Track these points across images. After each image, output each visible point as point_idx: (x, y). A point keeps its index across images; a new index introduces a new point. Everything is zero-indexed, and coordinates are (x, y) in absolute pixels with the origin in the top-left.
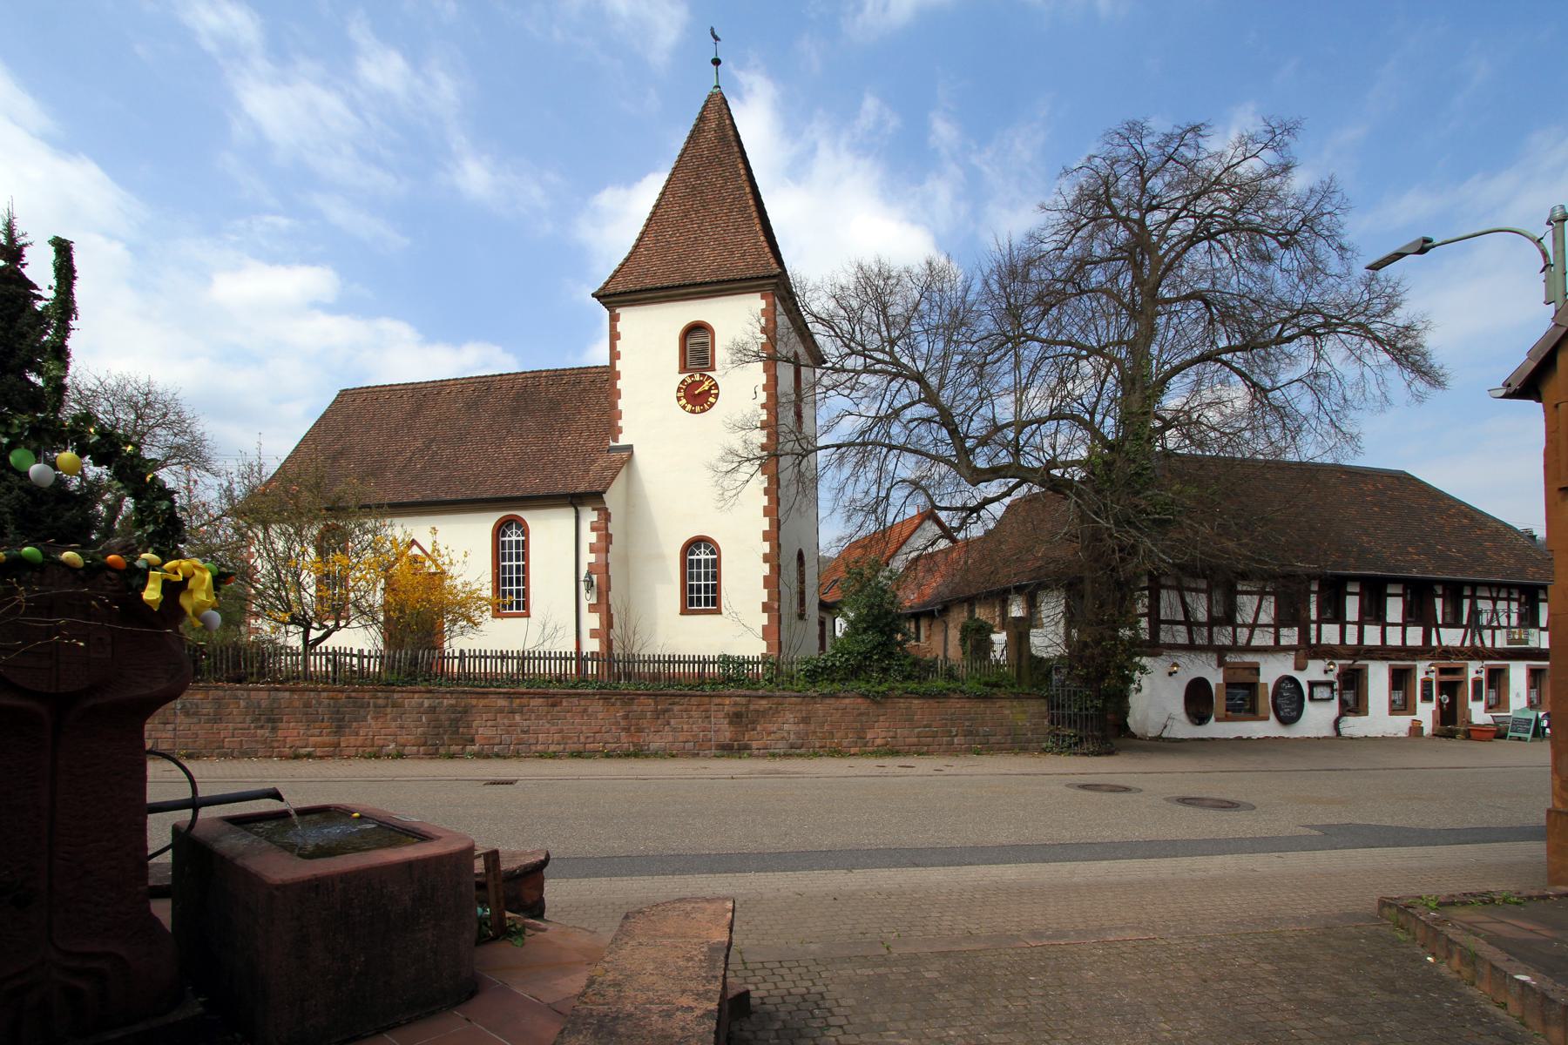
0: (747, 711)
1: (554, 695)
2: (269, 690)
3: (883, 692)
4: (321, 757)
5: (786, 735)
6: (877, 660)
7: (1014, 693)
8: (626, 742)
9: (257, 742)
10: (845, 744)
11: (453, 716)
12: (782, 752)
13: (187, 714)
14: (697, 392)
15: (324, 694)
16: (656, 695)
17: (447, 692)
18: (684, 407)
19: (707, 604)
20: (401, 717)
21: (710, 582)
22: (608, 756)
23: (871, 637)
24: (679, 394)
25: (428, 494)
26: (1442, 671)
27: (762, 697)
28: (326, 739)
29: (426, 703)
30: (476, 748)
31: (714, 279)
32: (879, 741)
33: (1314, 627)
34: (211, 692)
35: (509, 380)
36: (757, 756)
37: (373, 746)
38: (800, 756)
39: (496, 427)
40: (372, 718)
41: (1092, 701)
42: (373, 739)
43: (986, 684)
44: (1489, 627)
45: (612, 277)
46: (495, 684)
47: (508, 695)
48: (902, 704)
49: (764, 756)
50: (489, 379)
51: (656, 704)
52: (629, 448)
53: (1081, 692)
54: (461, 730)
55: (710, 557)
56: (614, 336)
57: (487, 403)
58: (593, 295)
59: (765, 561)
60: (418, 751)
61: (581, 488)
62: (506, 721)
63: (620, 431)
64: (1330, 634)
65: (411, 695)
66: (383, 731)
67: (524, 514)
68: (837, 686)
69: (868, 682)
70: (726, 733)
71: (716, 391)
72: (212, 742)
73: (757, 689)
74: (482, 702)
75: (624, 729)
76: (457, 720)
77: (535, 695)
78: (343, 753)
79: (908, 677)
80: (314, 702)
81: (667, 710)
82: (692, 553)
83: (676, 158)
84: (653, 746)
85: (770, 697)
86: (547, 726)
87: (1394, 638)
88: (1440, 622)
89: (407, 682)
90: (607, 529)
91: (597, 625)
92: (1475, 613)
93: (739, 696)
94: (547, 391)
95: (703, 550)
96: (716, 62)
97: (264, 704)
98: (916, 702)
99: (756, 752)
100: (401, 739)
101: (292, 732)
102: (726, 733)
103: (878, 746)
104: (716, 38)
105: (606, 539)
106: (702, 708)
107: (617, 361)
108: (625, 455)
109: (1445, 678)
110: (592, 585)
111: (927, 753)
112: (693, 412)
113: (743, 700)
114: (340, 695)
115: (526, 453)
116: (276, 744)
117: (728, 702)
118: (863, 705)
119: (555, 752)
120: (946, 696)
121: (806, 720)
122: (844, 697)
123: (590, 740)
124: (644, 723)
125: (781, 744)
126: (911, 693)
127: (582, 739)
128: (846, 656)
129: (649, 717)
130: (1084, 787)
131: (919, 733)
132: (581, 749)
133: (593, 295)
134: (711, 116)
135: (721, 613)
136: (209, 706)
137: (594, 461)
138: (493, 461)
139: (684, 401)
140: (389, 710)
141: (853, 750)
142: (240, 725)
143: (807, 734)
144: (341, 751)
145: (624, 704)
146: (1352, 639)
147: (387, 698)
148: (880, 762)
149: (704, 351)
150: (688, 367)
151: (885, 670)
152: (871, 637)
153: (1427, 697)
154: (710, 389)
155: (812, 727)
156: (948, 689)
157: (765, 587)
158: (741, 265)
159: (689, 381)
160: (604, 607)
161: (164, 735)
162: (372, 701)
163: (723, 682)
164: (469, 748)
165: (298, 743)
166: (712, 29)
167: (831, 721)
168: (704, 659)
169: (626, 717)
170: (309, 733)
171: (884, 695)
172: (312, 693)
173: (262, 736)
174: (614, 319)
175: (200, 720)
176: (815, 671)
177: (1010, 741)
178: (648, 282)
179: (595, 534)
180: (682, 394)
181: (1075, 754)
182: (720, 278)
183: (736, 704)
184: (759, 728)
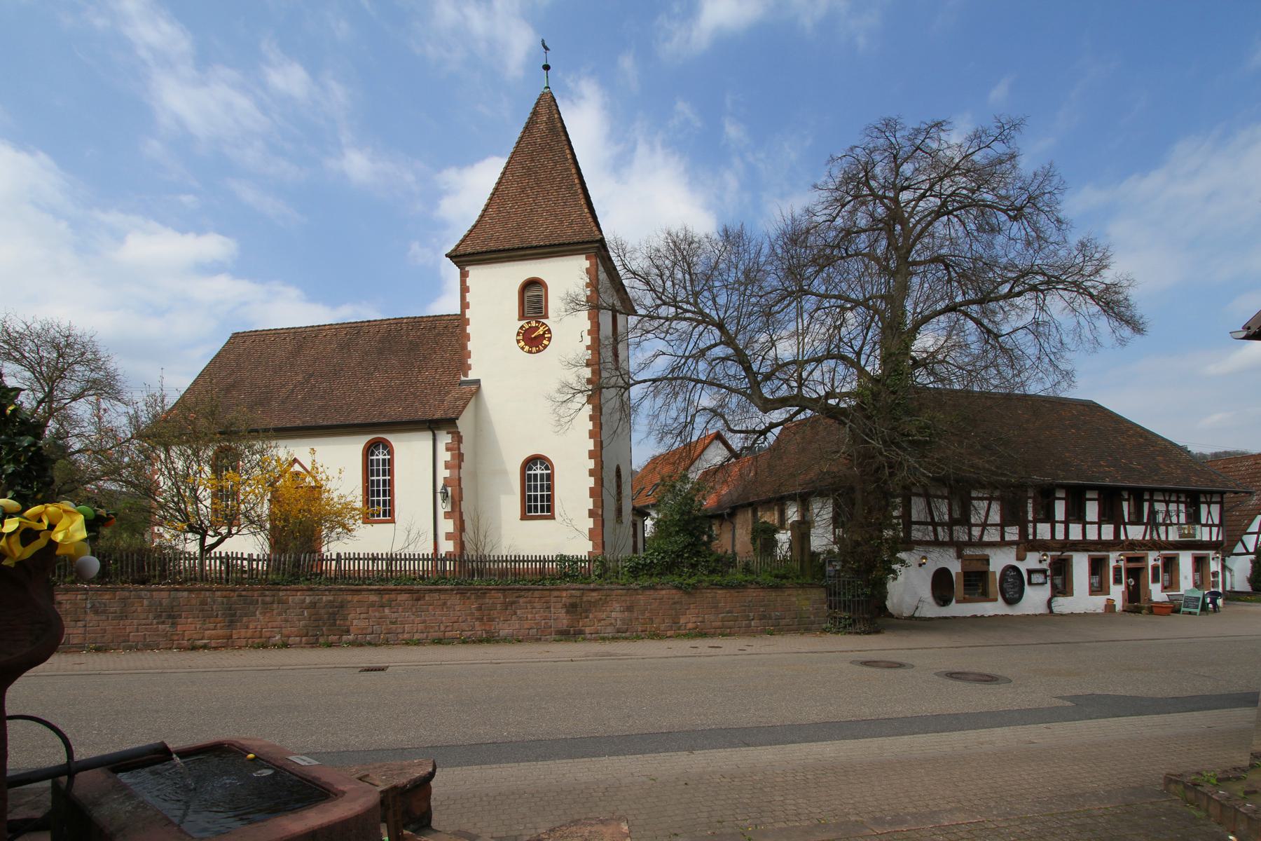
1: (418, 591)
2: (169, 590)
3: (693, 584)
4: (216, 648)
5: (613, 621)
6: (687, 558)
8: (479, 630)
9: (158, 635)
10: (662, 628)
11: (331, 610)
12: (610, 636)
13: (96, 612)
14: (533, 336)
15: (219, 593)
16: (504, 590)
17: (326, 590)
18: (522, 348)
19: (542, 511)
20: (286, 612)
21: (545, 493)
23: (682, 539)
24: (519, 338)
25: (308, 420)
26: (1129, 560)
27: (593, 590)
29: (308, 600)
30: (351, 637)
32: (690, 625)
33: (1031, 525)
36: (590, 640)
37: (261, 637)
38: (626, 638)
39: (365, 364)
40: (261, 613)
43: (776, 576)
44: (1164, 524)
45: (463, 241)
48: (709, 594)
49: (595, 640)
50: (359, 325)
52: (477, 382)
54: (338, 622)
55: (545, 472)
56: (464, 290)
58: (447, 256)
60: (301, 641)
61: (438, 415)
62: (377, 614)
64: (1043, 531)
65: (294, 593)
66: (270, 624)
67: (390, 437)
68: (655, 580)
70: (563, 620)
71: (549, 335)
73: (589, 584)
74: (356, 598)
76: (334, 614)
81: (513, 603)
82: (530, 469)
84: (502, 633)
87: (1092, 534)
88: (1126, 520)
90: (459, 449)
92: (1153, 513)
93: (574, 589)
95: (539, 466)
96: (547, 67)
97: (165, 602)
99: (589, 636)
101: (190, 626)
102: (563, 620)
103: (690, 629)
106: (543, 600)
107: (467, 310)
108: (474, 387)
109: (1131, 565)
110: (447, 496)
111: (729, 635)
112: (530, 352)
113: (578, 593)
114: (232, 594)
115: (391, 386)
117: (565, 595)
118: (677, 595)
120: (744, 587)
121: (629, 609)
122: (662, 589)
124: (495, 614)
125: (609, 629)
126: (716, 585)
127: (442, 628)
130: (866, 663)
132: (441, 637)
135: (554, 519)
139: (522, 343)
140: (275, 606)
141: (669, 633)
142: (144, 622)
143: (631, 620)
144: (233, 642)
146: (1060, 535)
149: (539, 302)
150: (526, 315)
151: (693, 566)
153: (1118, 581)
154: (544, 333)
155: (635, 615)
156: (746, 581)
159: (527, 327)
160: (457, 514)
162: (260, 599)
163: (560, 578)
164: (345, 638)
165: (195, 636)
169: (479, 609)
170: (205, 627)
171: (694, 587)
174: (464, 275)
178: (493, 245)
179: (449, 453)
180: (521, 337)
181: (850, 633)
183: (571, 596)
184: (591, 616)
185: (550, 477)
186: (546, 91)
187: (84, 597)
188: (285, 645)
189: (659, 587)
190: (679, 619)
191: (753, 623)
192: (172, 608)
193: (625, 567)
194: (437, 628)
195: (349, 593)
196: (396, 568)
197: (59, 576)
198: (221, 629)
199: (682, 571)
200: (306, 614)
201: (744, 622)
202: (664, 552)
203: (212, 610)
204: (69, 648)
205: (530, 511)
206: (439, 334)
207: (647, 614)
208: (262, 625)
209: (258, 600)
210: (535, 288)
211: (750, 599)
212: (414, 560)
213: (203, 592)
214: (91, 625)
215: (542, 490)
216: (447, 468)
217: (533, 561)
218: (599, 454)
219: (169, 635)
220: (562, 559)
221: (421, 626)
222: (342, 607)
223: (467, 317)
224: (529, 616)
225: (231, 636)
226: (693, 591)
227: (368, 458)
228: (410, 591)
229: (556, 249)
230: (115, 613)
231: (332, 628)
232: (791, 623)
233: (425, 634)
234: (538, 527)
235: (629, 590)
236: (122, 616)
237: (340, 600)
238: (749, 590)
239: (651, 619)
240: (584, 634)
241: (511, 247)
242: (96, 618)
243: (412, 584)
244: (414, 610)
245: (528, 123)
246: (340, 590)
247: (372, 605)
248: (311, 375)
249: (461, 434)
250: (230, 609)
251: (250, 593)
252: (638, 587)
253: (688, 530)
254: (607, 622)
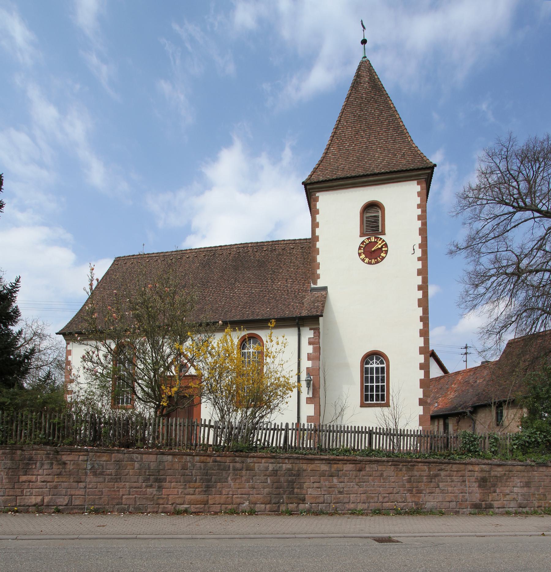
2: (157, 454)
9: (146, 498)
11: (290, 478)
13: (95, 474)
14: (373, 249)
15: (197, 458)
16: (429, 463)
17: (286, 458)
18: (363, 260)
22: (398, 513)
24: (360, 251)
29: (271, 467)
34: (113, 455)
35: (227, 249)
39: (226, 277)
40: (232, 479)
42: (232, 497)
45: (314, 172)
49: (502, 514)
50: (214, 249)
52: (325, 289)
54: (296, 490)
55: (380, 366)
57: (215, 263)
61: (304, 313)
62: (327, 483)
63: (318, 277)
65: (260, 460)
66: (239, 491)
67: (263, 334)
71: (386, 249)
72: (114, 498)
74: (310, 467)
76: (293, 482)
78: (211, 510)
80: (189, 464)
81: (436, 476)
82: (367, 363)
84: (428, 505)
86: (356, 487)
93: (484, 464)
94: (255, 256)
95: (375, 361)
97: (153, 466)
100: (253, 498)
105: (317, 349)
107: (317, 229)
108: (323, 293)
112: (369, 263)
113: (487, 468)
115: (253, 293)
121: (527, 485)
123: (386, 499)
125: (513, 504)
129: (425, 480)
132: (380, 508)
134: (364, 74)
136: (111, 467)
138: (231, 298)
139: (363, 256)
140: (244, 472)
142: (135, 484)
144: (209, 508)
145: (409, 470)
149: (377, 221)
154: (382, 247)
157: (421, 387)
159: (367, 242)
161: (77, 493)
162: (231, 465)
164: (301, 506)
165: (179, 501)
166: (362, 21)
169: (409, 481)
170: (186, 491)
172: (188, 457)
175: (105, 479)
178: (340, 174)
179: (311, 347)
180: (362, 251)
183: (482, 471)
186: (364, 59)
187: (86, 458)
188: (252, 513)
192: (159, 472)
195: (305, 462)
196: (310, 442)
197: (58, 437)
198: (199, 494)
200: (269, 481)
203: (192, 475)
204: (72, 509)
205: (367, 400)
206: (279, 254)
207: (541, 491)
208: (233, 492)
210: (373, 210)
213: (184, 457)
214: (90, 486)
216: (309, 359)
221: (363, 497)
222: (299, 475)
223: (317, 234)
225: (208, 501)
228: (354, 462)
229: (394, 176)
230: (111, 475)
236: (116, 478)
237: (296, 469)
242: (95, 479)
245: (353, 83)
247: (323, 474)
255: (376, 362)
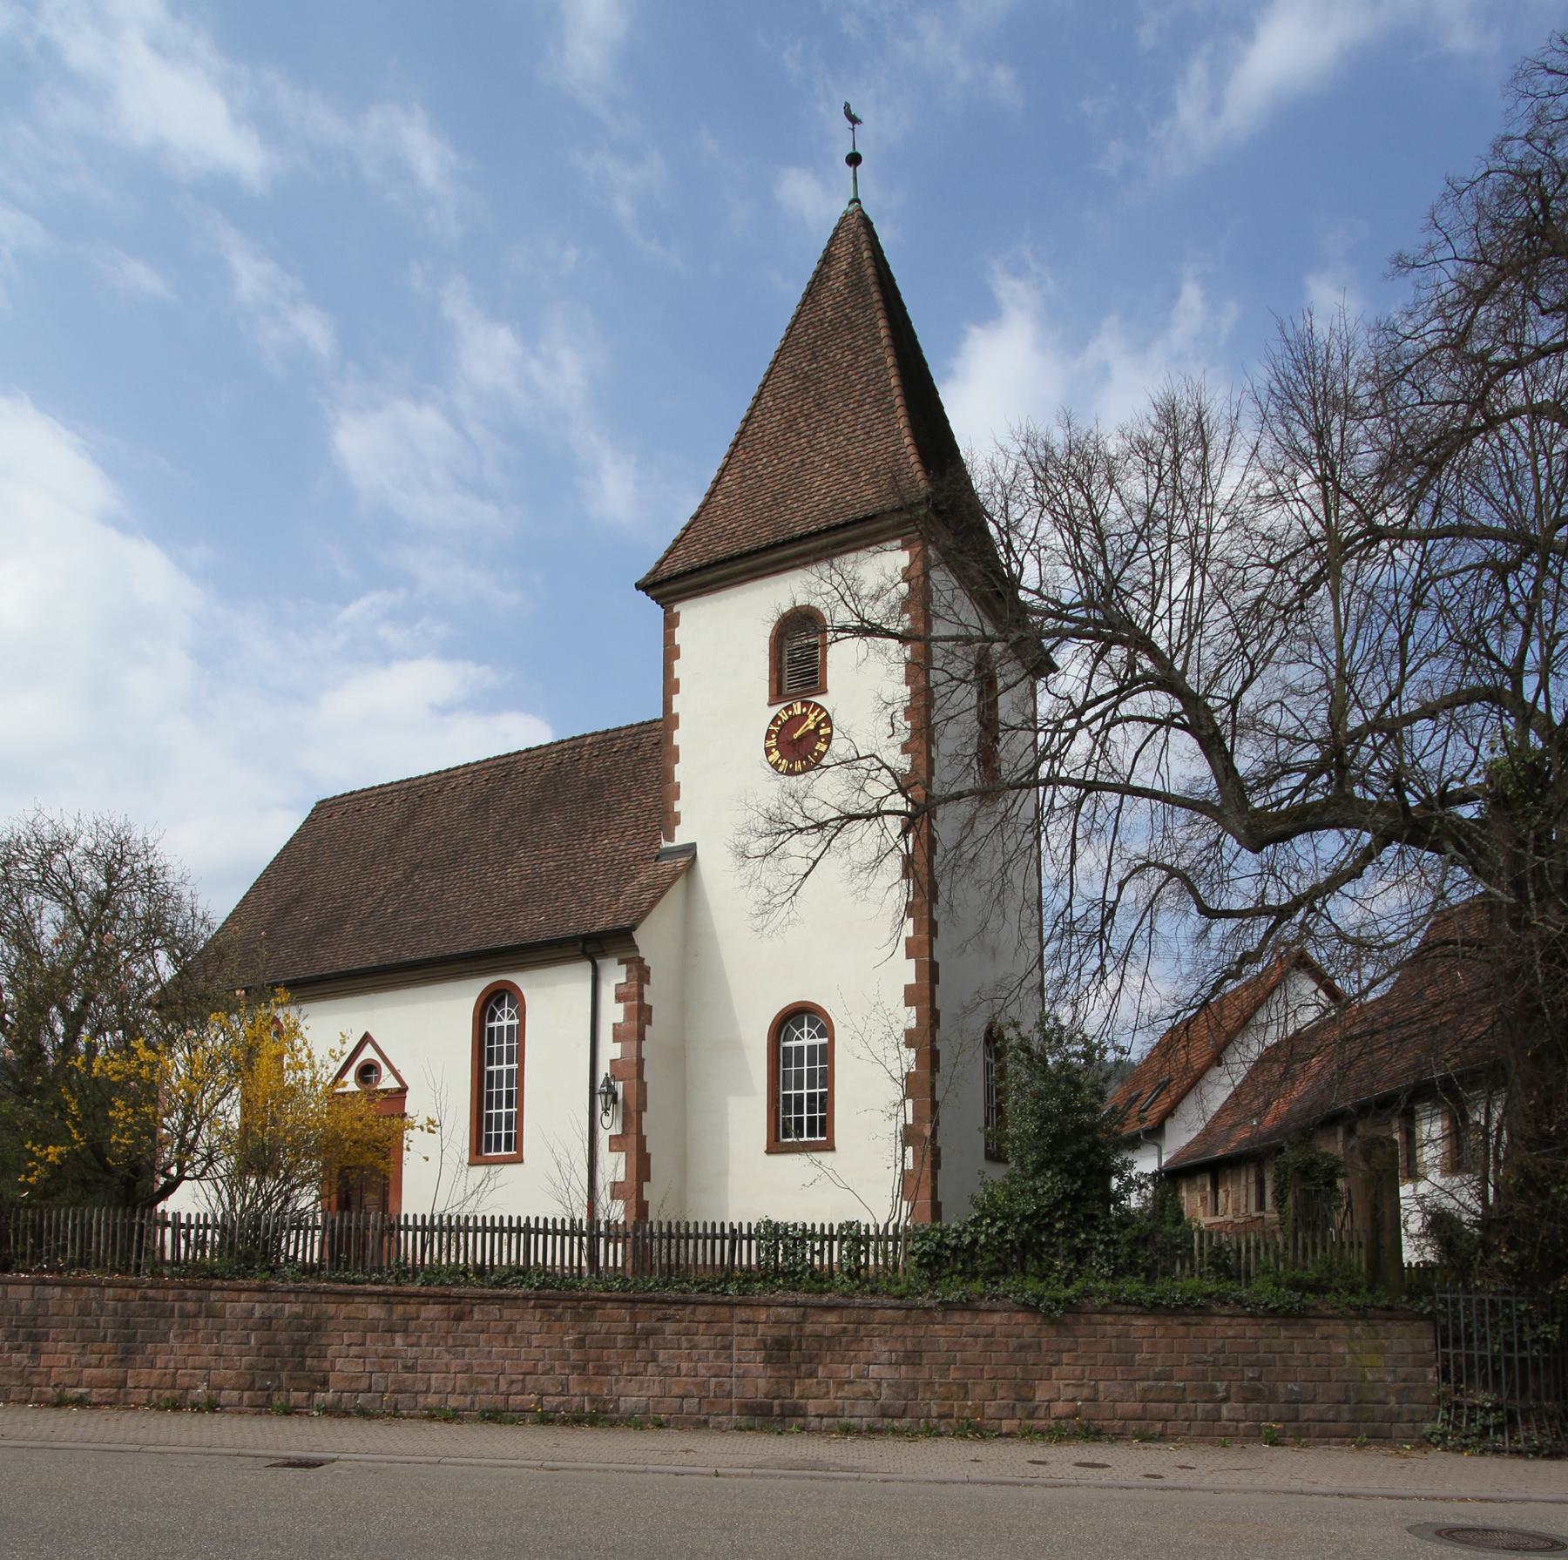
0: (800, 1337)
1: (461, 1298)
2: (33, 1284)
3: (1067, 1299)
4: (96, 1405)
5: (872, 1388)
6: (1064, 1232)
7: (1357, 1308)
8: (578, 1396)
9: (9, 1374)
10: (990, 1411)
11: (297, 1335)
12: (865, 1422)
14: (796, 736)
15: (110, 1292)
17: (289, 1291)
20: (218, 1335)
21: (818, 1090)
23: (1048, 1182)
25: (390, 955)
27: (829, 1308)
28: (107, 1372)
30: (329, 1396)
31: (823, 526)
32: (1060, 1408)
36: (817, 1431)
37: (173, 1387)
38: (897, 1432)
41: (1533, 1327)
43: (1296, 1285)
45: (670, 551)
46: (375, 1276)
47: (387, 1298)
48: (1109, 1326)
49: (828, 1431)
50: (512, 759)
51: (634, 1321)
52: (690, 850)
53: (1506, 1304)
54: (309, 1361)
55: (819, 1041)
58: (638, 586)
59: (909, 1044)
60: (241, 1398)
62: (380, 1348)
63: (676, 820)
65: (234, 1295)
67: (520, 979)
68: (977, 1286)
69: (1043, 1277)
70: (757, 1379)
71: (828, 730)
73: (822, 1292)
74: (344, 1310)
75: (574, 1367)
76: (302, 1343)
77: (428, 1298)
79: (1130, 1268)
81: (650, 1333)
83: (783, 334)
84: (626, 1404)
85: (846, 1307)
86: (447, 1357)
89: (237, 1272)
90: (641, 996)
91: (621, 1176)
93: (784, 1305)
94: (590, 767)
95: (806, 1028)
96: (854, 160)
97: (25, 1306)
98: (1139, 1322)
99: (814, 1422)
100: (216, 1377)
101: (60, 1358)
102: (757, 1379)
103: (1058, 1418)
104: (854, 120)
106: (716, 1328)
107: (674, 697)
108: (681, 861)
110: (615, 1100)
111: (1161, 1437)
113: (792, 1314)
114: (132, 1293)
115: (539, 875)
116: (36, 1380)
117: (763, 1317)
118: (1028, 1327)
119: (456, 1410)
120: (1202, 1310)
121: (912, 1358)
122: (990, 1311)
123: (517, 1387)
124: (612, 1357)
125: (863, 1407)
126: (1127, 1303)
127: (503, 1387)
128: (1000, 1224)
130: (1451, 1534)
131: (1145, 1391)
132: (501, 1406)
133: (638, 586)
135: (833, 1149)
137: (633, 877)
139: (776, 755)
140: (201, 1321)
141: (1006, 1426)
143: (914, 1387)
144: (126, 1394)
147: (200, 1300)
148: (1038, 1451)
149: (811, 659)
150: (785, 691)
151: (1080, 1255)
152: (1048, 1182)
154: (818, 727)
155: (925, 1373)
156: (1209, 1296)
158: (869, 493)
159: (785, 718)
160: (633, 1140)
162: (177, 1305)
163: (764, 1278)
164: (319, 1396)
165: (68, 1379)
167: (963, 1362)
168: (733, 1231)
169: (580, 1344)
170: (84, 1360)
171: (1071, 1307)
173: (19, 1364)
174: (671, 622)
176: (937, 1256)
177: (1347, 1417)
179: (621, 1006)
180: (773, 742)
181: (1497, 1452)
182: (833, 522)
184: (821, 1372)
185: (827, 1053)
188: (212, 1407)
189: (984, 1305)
190: (1032, 1387)
191: (1225, 1410)
192: (35, 1320)
193: (913, 1253)
194: (492, 1384)
195: (332, 1298)
198: (109, 1366)
199: (1051, 1266)
201: (1200, 1405)
202: (1005, 1217)
203: (98, 1327)
207: (953, 1374)
209: (173, 1308)
211: (1219, 1343)
212: (546, 1232)
213: (85, 1289)
215: (811, 1085)
217: (706, 1237)
218: (926, 993)
219: (26, 1373)
220: (773, 1233)
224: (684, 1366)
226: (1069, 1318)
227: (779, 1045)
228: (444, 1299)
229: (841, 537)
231: (296, 1374)
232: (1331, 1415)
233: (469, 1397)
234: (794, 1165)
235: (910, 1309)
238: (1217, 1320)
239: (964, 1387)
240: (804, 1416)
241: (754, 546)
243: (456, 1283)
244: (450, 1341)
245: (812, 283)
246: (315, 1291)
248: (417, 867)
249: (647, 963)
250: (127, 1325)
251: (160, 1294)
252: (932, 1303)
253: (1062, 1160)
254: (857, 1389)
255: (809, 1032)
